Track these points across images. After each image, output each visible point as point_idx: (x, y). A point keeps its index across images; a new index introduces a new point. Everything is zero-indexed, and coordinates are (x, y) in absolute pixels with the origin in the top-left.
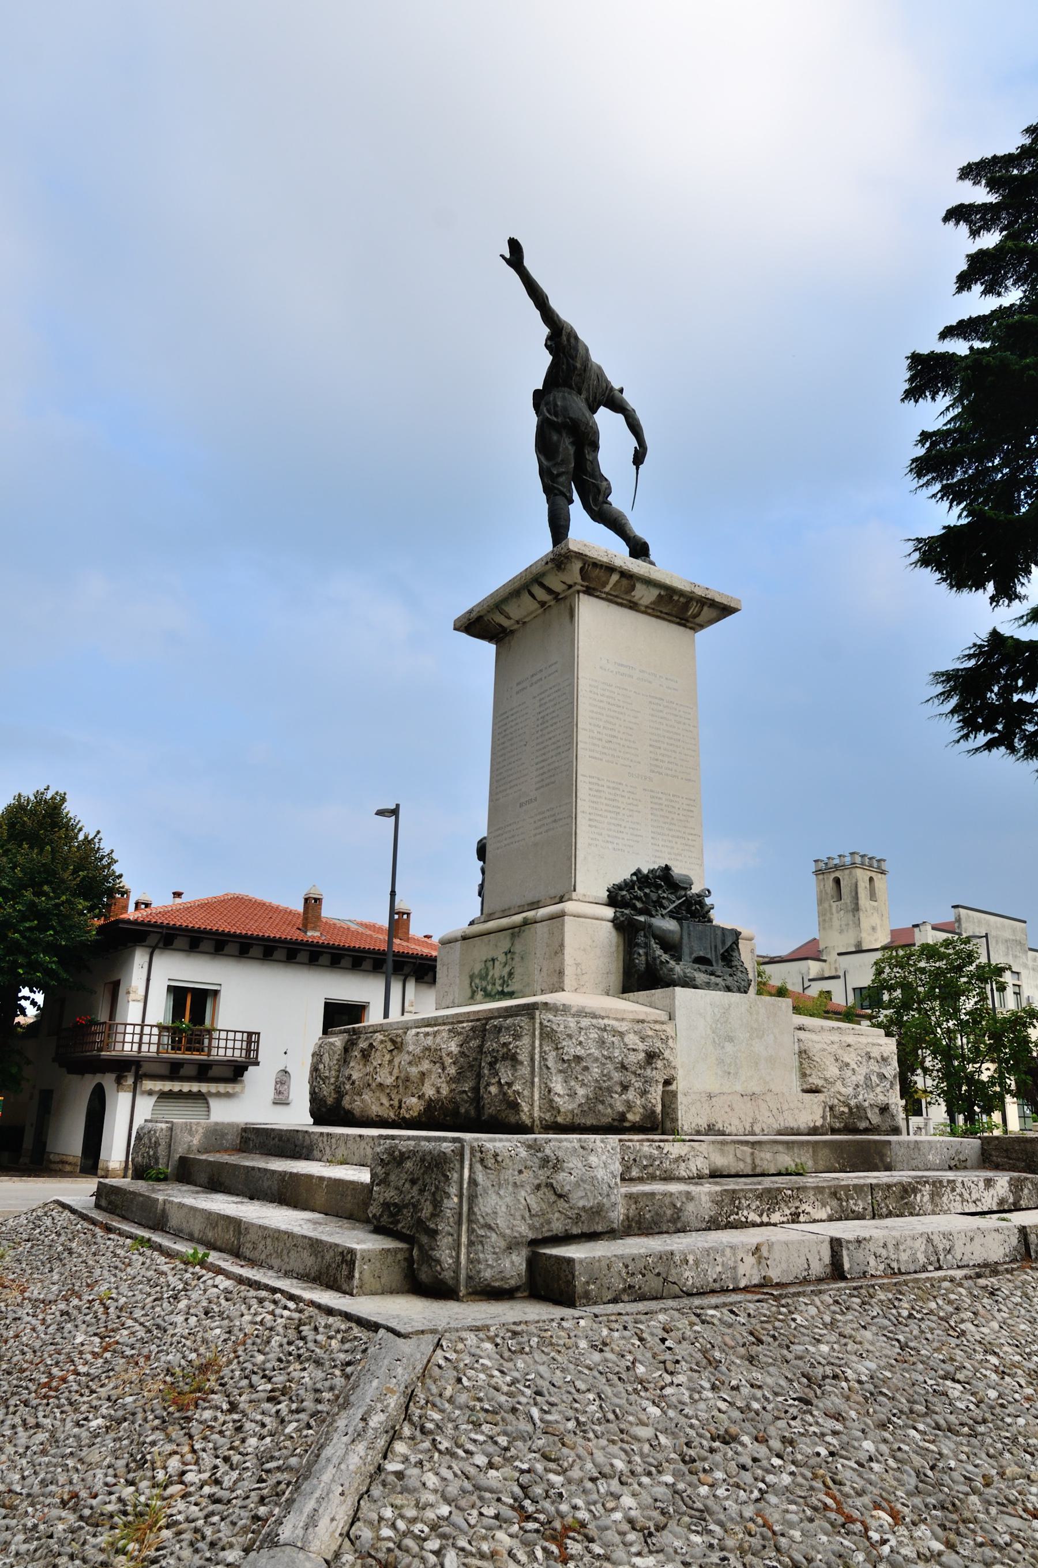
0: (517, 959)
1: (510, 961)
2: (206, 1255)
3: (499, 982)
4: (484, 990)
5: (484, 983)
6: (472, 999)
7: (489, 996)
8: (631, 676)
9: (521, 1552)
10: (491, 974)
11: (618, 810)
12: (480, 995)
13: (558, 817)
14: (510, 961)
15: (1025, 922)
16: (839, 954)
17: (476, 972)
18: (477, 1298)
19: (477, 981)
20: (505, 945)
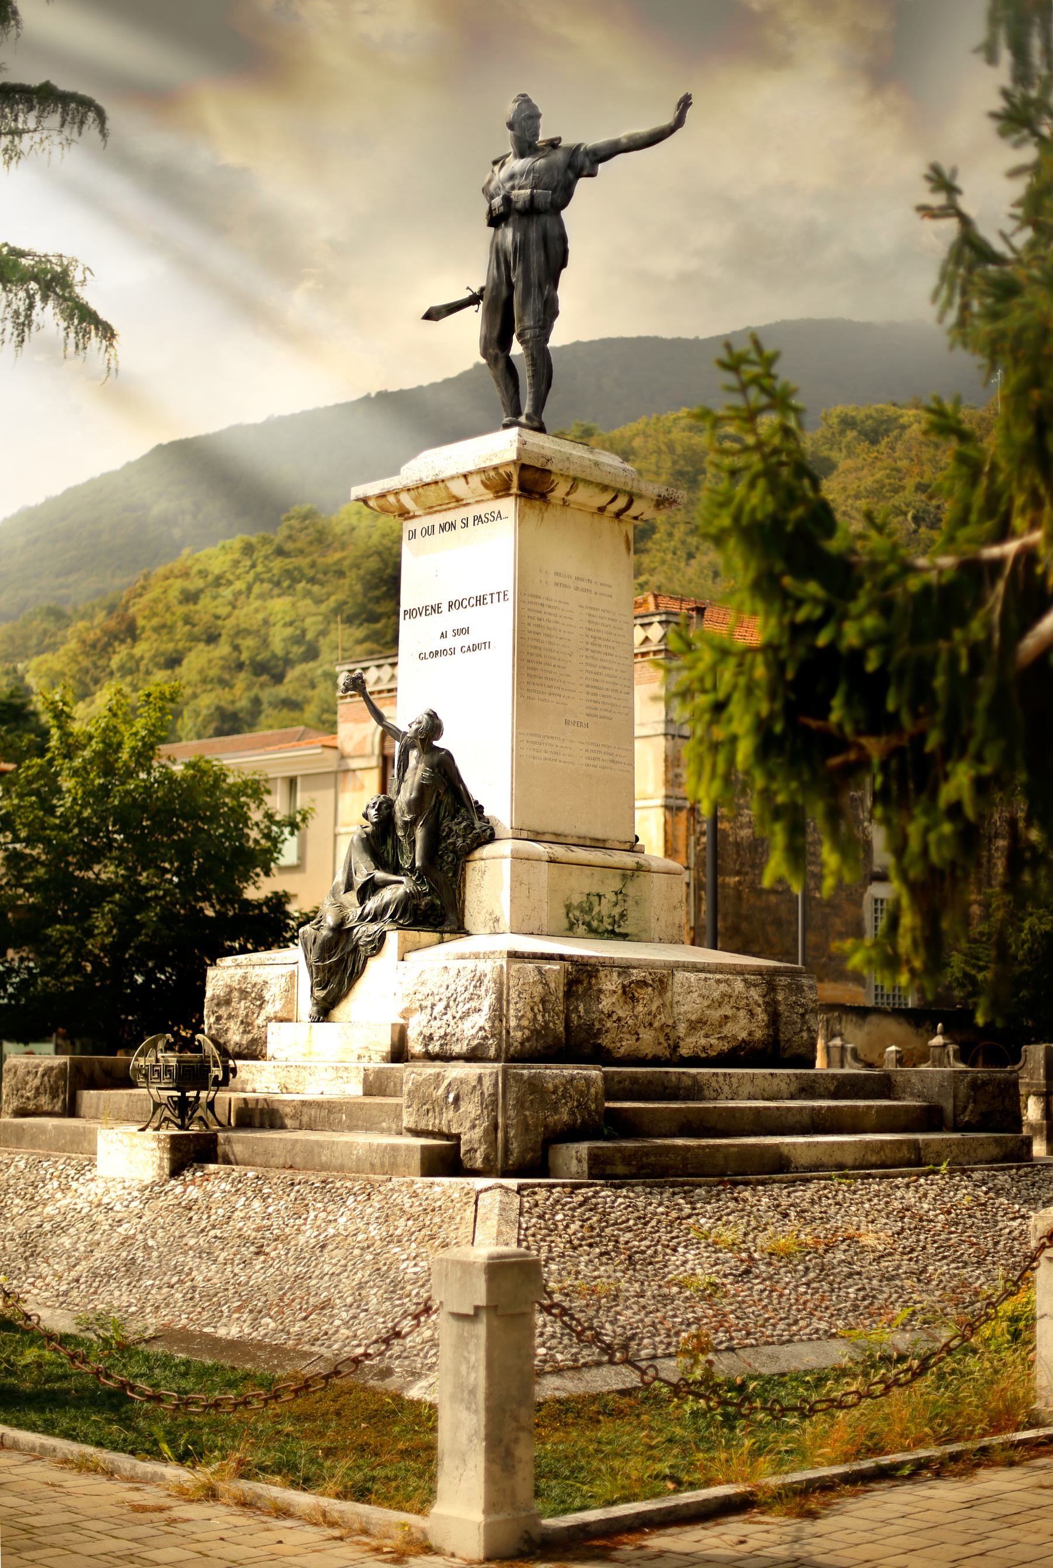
0: (630, 902)
1: (621, 903)
2: (783, 574)
3: (607, 921)
4: (589, 925)
5: (587, 918)
6: (570, 930)
7: (594, 933)
8: (557, 574)
9: (128, 1466)
10: (596, 909)
11: (559, 580)
12: (581, 929)
13: (617, 759)
14: (621, 903)
15: (432, 315)
16: (432, 315)
17: (575, 904)
18: (396, 1038)
19: (577, 913)
20: (617, 885)
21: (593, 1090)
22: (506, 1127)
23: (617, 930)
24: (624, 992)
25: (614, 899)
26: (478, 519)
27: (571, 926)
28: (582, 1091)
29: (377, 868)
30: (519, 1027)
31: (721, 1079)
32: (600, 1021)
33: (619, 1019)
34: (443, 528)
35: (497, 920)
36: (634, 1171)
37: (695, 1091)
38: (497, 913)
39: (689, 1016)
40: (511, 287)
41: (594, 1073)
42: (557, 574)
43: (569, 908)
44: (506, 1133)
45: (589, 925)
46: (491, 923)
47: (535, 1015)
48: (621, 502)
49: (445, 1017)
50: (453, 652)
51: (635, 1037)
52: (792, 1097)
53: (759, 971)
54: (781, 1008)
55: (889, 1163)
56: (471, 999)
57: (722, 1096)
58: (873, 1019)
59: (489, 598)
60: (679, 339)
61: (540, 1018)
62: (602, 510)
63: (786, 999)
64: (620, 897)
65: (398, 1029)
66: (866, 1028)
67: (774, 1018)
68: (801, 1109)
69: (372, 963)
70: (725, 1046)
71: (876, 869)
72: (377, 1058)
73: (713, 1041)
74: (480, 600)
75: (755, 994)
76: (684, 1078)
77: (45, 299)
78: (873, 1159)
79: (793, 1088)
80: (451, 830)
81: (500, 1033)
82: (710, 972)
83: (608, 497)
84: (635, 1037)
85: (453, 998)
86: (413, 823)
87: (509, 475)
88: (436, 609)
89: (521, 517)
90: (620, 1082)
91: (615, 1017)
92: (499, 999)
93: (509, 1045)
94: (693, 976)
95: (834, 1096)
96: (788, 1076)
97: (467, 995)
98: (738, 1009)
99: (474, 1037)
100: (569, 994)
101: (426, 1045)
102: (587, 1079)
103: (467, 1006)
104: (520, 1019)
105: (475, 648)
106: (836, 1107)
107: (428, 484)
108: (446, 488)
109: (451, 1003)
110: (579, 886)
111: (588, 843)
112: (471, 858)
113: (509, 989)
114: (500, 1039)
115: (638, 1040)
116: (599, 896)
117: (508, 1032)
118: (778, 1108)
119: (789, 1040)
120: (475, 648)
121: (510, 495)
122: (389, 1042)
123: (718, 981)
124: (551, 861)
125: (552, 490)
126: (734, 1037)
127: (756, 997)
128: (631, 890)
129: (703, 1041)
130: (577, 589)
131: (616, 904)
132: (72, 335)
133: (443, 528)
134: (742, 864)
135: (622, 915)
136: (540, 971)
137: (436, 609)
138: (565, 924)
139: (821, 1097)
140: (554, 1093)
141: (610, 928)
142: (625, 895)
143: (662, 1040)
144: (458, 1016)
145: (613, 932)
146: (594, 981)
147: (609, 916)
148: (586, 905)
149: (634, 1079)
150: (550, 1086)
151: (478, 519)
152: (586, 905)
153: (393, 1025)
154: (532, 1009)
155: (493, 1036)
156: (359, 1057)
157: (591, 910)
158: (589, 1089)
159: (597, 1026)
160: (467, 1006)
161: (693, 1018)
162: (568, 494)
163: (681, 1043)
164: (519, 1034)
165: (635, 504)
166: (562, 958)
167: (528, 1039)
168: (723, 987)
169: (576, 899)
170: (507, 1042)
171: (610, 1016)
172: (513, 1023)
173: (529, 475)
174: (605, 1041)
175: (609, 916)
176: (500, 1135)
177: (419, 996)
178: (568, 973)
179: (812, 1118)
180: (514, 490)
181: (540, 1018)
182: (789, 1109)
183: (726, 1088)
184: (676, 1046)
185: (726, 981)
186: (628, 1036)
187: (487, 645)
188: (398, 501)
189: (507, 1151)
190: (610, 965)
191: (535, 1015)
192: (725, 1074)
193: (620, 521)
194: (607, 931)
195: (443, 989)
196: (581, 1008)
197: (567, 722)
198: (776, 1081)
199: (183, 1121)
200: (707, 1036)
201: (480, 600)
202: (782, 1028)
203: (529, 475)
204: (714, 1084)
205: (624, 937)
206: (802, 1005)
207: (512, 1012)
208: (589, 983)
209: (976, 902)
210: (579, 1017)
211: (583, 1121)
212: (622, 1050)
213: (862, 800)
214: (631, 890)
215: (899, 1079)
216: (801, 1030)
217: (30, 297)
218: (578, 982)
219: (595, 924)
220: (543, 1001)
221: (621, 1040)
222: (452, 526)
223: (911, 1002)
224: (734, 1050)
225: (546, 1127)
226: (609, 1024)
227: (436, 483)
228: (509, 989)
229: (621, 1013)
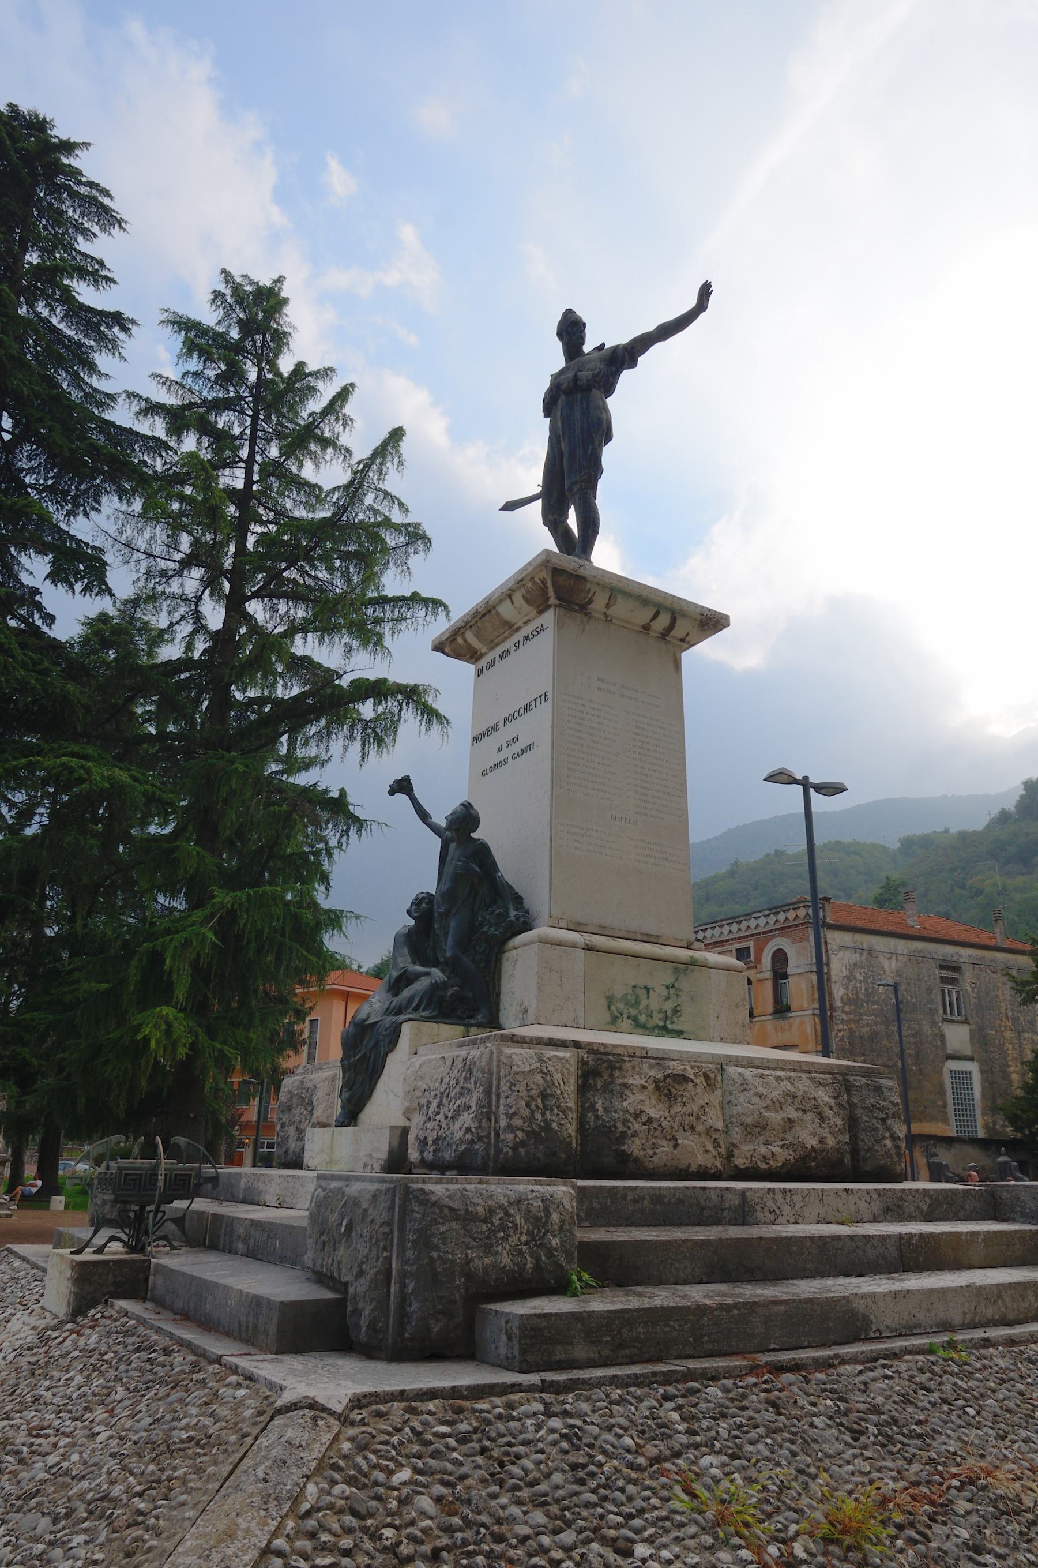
4: (635, 1019)
5: (633, 1012)
8: (599, 680)
10: (644, 1003)
17: (619, 996)
18: (396, 1144)
19: (621, 1006)
20: (669, 980)
21: (555, 1217)
22: (403, 1275)
23: (670, 1027)
24: (658, 1088)
25: (665, 993)
26: (526, 638)
27: (614, 1020)
28: (537, 1219)
29: (414, 963)
30: (510, 1128)
31: (779, 1196)
32: (625, 1122)
33: (650, 1120)
34: (501, 657)
35: (526, 1011)
36: (606, 1352)
37: (744, 1213)
38: (526, 1004)
39: (743, 1118)
40: (562, 454)
41: (561, 1190)
42: (599, 680)
43: (610, 1001)
44: (403, 1286)
45: (635, 1019)
46: (521, 1016)
47: (532, 1113)
48: (663, 621)
49: (438, 1117)
50: (506, 761)
51: (672, 1143)
52: (875, 1220)
53: (829, 1071)
54: (859, 1112)
55: (1011, 1316)
56: (461, 1094)
57: (781, 1219)
58: (957, 1145)
59: (533, 704)
60: (665, 340)
61: (539, 1117)
62: (646, 628)
63: (863, 1101)
64: (672, 991)
65: (399, 1132)
66: (953, 1151)
67: (852, 1123)
68: (884, 1238)
69: (390, 1058)
70: (790, 1155)
71: (949, 1052)
72: (377, 1167)
73: (776, 1150)
74: (527, 708)
75: (824, 1096)
76: (728, 1195)
77: (408, 704)
78: (990, 1312)
79: (876, 1207)
80: (484, 918)
81: (488, 1136)
82: (769, 1068)
83: (647, 614)
84: (672, 1143)
85: (445, 1094)
86: (447, 914)
87: (544, 581)
88: (495, 728)
89: (559, 624)
90: (635, 1201)
91: (644, 1119)
92: (488, 1092)
93: (498, 1151)
94: (748, 1073)
95: (929, 1218)
96: (868, 1192)
97: (457, 1089)
98: (805, 1111)
99: (462, 1141)
100: (584, 1088)
101: (422, 1152)
102: (548, 1202)
103: (459, 1102)
104: (510, 1117)
105: (523, 751)
106: (932, 1235)
107: (484, 615)
108: (498, 613)
109: (444, 1100)
110: (622, 978)
111: (639, 937)
112: (506, 948)
113: (499, 1079)
114: (489, 1144)
115: (676, 1146)
116: (647, 989)
117: (497, 1134)
118: (852, 1238)
119: (870, 1149)
120: (523, 751)
121: (549, 607)
122: (385, 1148)
123: (778, 1079)
124: (588, 948)
125: (590, 602)
126: (803, 1146)
127: (827, 1099)
128: (684, 984)
129: (763, 1150)
130: (622, 696)
131: (668, 998)
132: (424, 723)
133: (501, 657)
134: (865, 1049)
135: (676, 1011)
136: (540, 1059)
137: (495, 728)
138: (607, 1017)
139: (911, 1218)
140: (485, 1221)
141: (661, 1024)
142: (679, 990)
143: (710, 1147)
144: (450, 1115)
145: (664, 1028)
146: (617, 1073)
147: (660, 1011)
148: (631, 999)
149: (657, 1197)
150: (480, 1210)
151: (526, 638)
152: (631, 999)
153: (392, 1128)
154: (528, 1105)
155: (480, 1139)
156: (365, 1167)
157: (637, 1003)
158: (548, 1214)
159: (621, 1128)
160: (459, 1102)
161: (749, 1121)
162: (608, 606)
163: (736, 1152)
164: (510, 1136)
165: (678, 622)
166: (577, 1045)
167: (523, 1143)
168: (786, 1085)
169: (619, 992)
170: (496, 1147)
171: (637, 1116)
172: (503, 1123)
173: (561, 580)
174: (634, 1147)
175: (660, 1011)
176: (394, 1288)
177: (418, 1093)
178: (582, 1063)
179: (900, 1249)
180: (553, 601)
181: (539, 1117)
182: (867, 1238)
183: (786, 1209)
184: (730, 1156)
185: (789, 1079)
186: (664, 1143)
187: (531, 746)
188: (465, 641)
189: (403, 1316)
190: (645, 1055)
191: (532, 1113)
192: (784, 1191)
193: (668, 642)
194: (658, 1027)
195: (437, 1084)
196: (599, 1106)
197: (613, 818)
198: (852, 1199)
199: (138, 1240)
200: (767, 1143)
201: (527, 708)
202: (862, 1135)
203: (561, 580)
204: (770, 1203)
205: (679, 1034)
206: (881, 1109)
207: (502, 1108)
208: (611, 1075)
209: (1015, 1072)
210: (597, 1117)
211: (538, 1266)
212: (655, 1159)
213: (936, 1010)
214: (684, 984)
215: (1005, 1195)
216: (884, 1138)
217: (401, 705)
218: (595, 1073)
219: (643, 1018)
220: (544, 1096)
221: (654, 1146)
222: (508, 652)
223: (981, 1134)
224: (803, 1159)
225: (469, 1276)
226: (637, 1126)
227: (489, 611)
228: (499, 1079)
229: (653, 1114)
